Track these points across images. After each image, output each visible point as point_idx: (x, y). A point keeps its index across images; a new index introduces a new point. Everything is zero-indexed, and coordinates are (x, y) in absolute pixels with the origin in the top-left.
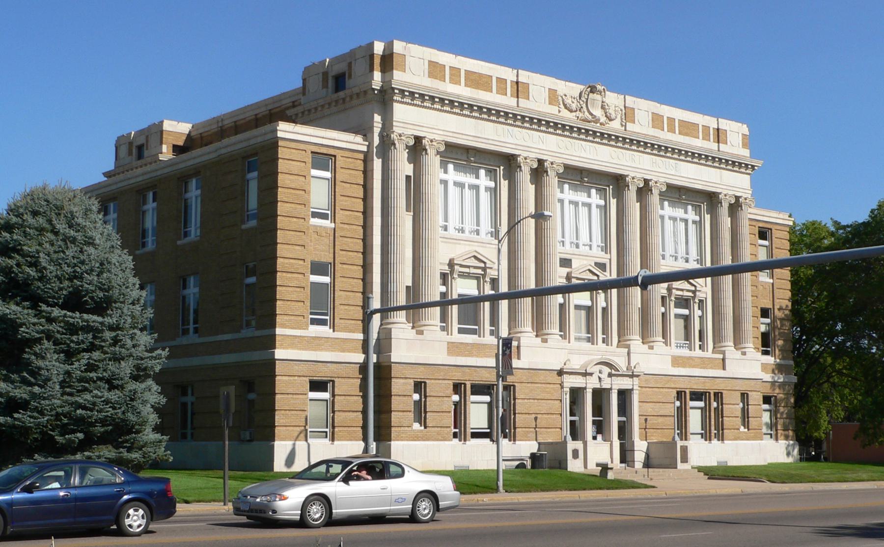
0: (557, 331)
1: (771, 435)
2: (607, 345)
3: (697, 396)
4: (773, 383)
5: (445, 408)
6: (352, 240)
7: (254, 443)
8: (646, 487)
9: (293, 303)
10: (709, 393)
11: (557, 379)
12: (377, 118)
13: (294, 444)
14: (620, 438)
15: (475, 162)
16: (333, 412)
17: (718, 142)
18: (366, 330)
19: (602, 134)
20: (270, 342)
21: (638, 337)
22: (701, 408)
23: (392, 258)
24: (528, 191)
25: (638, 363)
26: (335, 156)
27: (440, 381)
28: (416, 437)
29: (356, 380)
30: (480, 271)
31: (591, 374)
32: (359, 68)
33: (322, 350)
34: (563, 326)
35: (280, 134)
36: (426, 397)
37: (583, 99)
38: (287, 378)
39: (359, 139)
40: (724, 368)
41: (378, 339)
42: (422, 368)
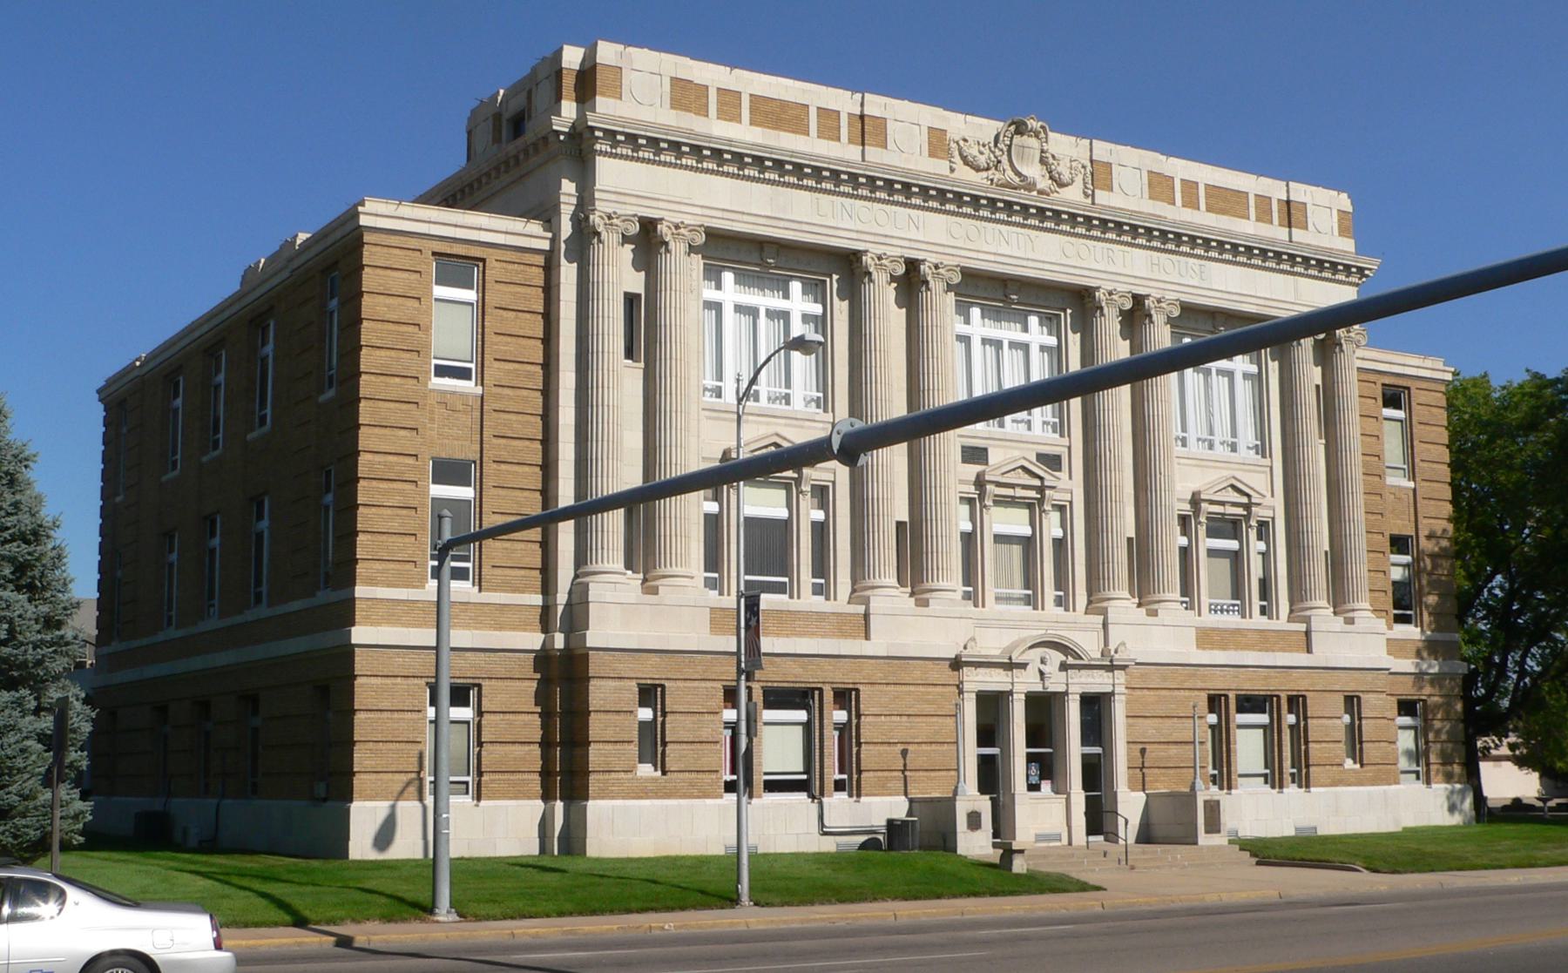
0: (1177, 595)
1: (1417, 773)
2: (1035, 608)
3: (1250, 703)
4: (1419, 676)
5: (705, 734)
6: (520, 417)
7: (328, 804)
8: (1084, 887)
9: (394, 538)
10: (1278, 697)
11: (950, 676)
12: (568, 187)
13: (393, 807)
14: (1086, 787)
15: (776, 268)
16: (480, 744)
17: (1290, 226)
18: (547, 586)
19: (1041, 211)
20: (345, 614)
21: (1324, 603)
22: (1263, 727)
23: (595, 448)
24: (888, 318)
25: (1123, 644)
26: (483, 260)
27: (696, 684)
28: (644, 791)
29: (527, 683)
30: (1033, 494)
31: (1023, 666)
32: (542, 96)
34: (1187, 588)
35: (364, 221)
36: (859, 716)
37: (1001, 145)
38: (378, 681)
39: (535, 227)
40: (1309, 651)
41: (569, 605)
42: (655, 658)
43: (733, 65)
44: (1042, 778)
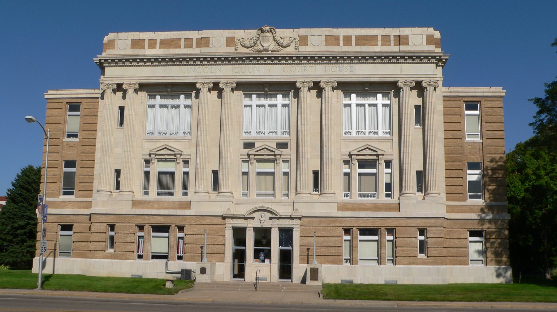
1: (482, 260)
11: (221, 221)
28: (424, 263)
33: (66, 208)
42: (112, 217)
43: (245, 29)
44: (266, 257)
